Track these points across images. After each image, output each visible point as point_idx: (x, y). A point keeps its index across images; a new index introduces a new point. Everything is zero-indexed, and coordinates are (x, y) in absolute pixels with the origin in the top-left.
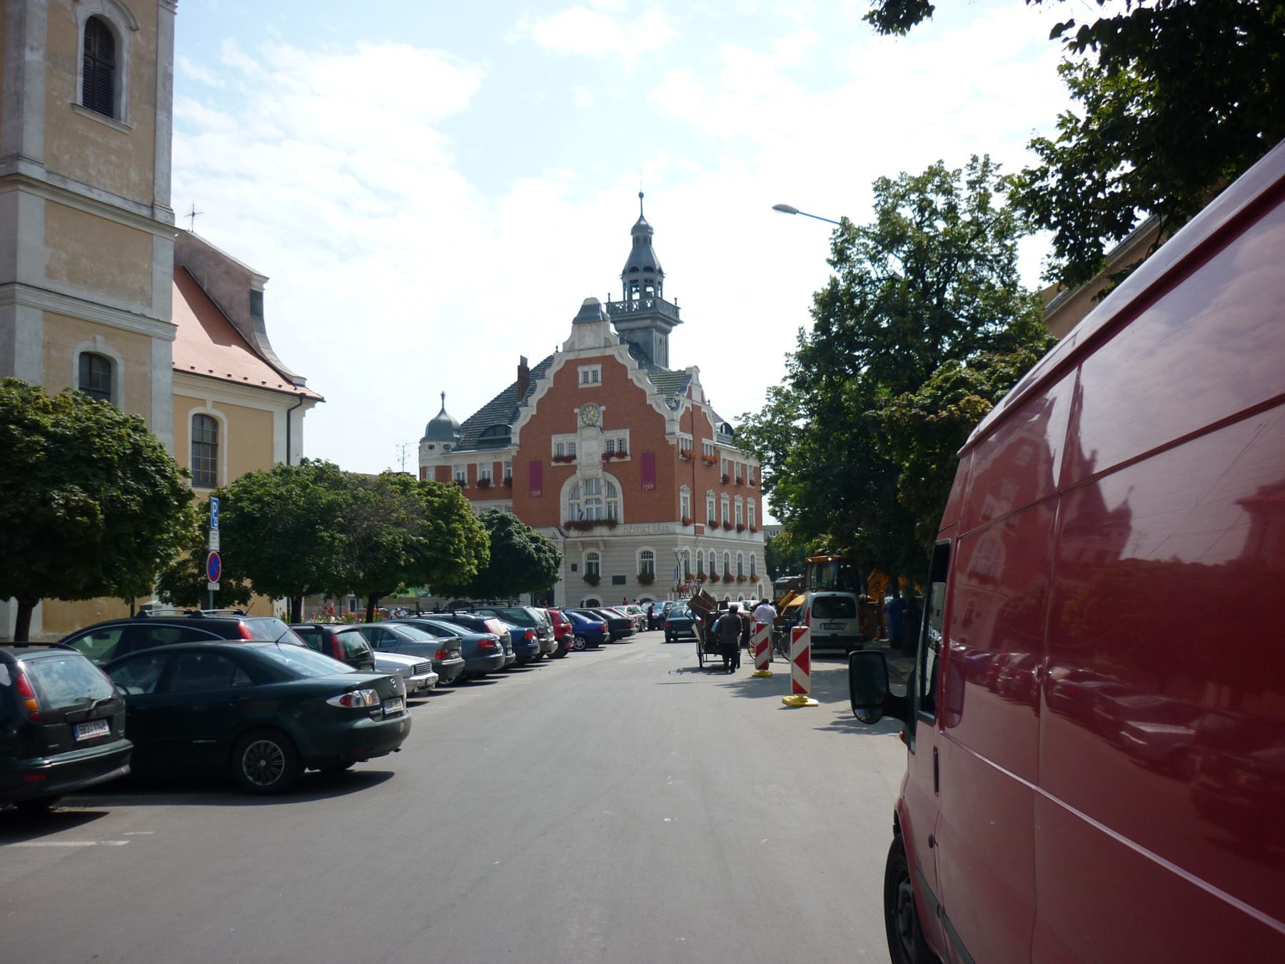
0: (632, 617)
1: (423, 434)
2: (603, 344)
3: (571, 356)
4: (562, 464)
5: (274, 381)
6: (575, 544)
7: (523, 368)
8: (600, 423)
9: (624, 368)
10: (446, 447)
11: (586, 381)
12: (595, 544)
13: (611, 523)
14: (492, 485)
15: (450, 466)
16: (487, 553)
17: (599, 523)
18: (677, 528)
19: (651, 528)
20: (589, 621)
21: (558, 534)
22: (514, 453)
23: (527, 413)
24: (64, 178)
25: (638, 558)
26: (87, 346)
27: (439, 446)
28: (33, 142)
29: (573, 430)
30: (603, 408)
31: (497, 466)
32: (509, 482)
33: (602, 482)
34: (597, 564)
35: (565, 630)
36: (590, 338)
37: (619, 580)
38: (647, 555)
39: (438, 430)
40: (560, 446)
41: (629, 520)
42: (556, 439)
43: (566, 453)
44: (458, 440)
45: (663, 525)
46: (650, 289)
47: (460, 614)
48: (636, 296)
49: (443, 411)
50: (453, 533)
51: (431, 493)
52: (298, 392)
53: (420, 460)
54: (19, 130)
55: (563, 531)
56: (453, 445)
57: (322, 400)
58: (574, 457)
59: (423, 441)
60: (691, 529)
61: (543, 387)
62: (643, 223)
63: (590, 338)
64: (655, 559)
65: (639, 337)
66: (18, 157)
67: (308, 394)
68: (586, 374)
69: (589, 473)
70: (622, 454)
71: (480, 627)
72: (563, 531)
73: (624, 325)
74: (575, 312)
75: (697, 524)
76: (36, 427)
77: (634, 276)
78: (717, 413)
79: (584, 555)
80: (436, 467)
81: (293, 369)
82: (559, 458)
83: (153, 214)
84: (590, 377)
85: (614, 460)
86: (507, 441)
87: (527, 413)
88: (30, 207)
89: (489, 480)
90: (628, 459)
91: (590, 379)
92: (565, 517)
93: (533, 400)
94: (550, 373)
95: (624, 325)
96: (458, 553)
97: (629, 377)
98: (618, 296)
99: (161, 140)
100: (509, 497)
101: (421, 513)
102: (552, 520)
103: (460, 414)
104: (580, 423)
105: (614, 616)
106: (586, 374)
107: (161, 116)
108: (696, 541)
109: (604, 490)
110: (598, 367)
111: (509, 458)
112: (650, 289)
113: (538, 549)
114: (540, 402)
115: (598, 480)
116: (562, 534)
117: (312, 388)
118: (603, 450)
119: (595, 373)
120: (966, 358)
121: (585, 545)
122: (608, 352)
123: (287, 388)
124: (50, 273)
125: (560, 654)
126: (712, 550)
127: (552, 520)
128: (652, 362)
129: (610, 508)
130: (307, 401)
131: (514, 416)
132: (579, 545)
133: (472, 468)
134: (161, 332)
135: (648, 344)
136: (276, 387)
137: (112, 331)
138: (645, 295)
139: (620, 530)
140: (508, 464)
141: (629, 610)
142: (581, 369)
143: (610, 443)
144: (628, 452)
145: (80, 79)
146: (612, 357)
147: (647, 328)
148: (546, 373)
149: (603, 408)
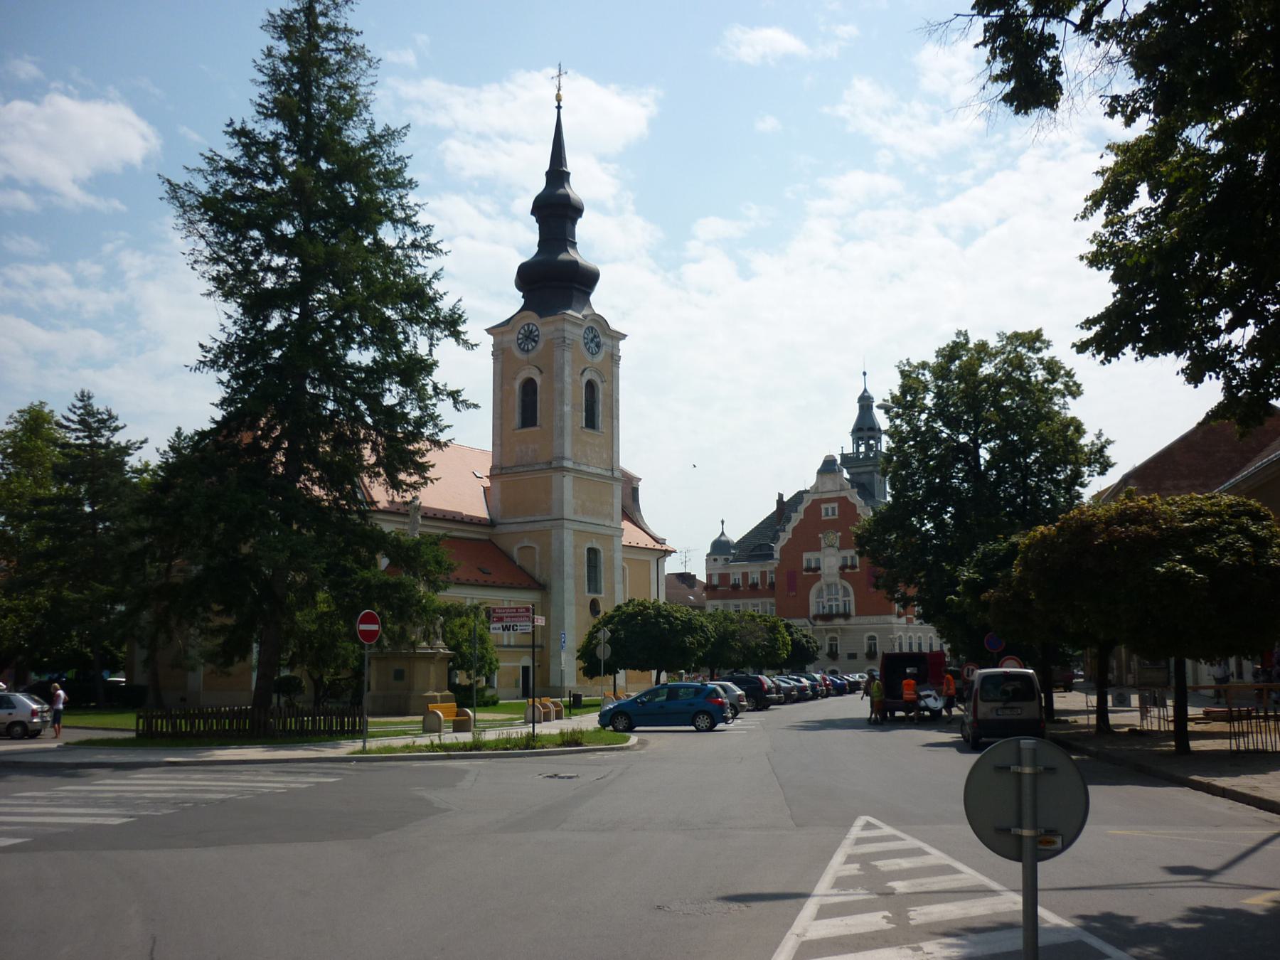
0: (861, 680)
1: (709, 551)
2: (838, 488)
3: (816, 497)
4: (810, 573)
5: (651, 544)
6: (821, 630)
7: (780, 501)
8: (837, 544)
9: (854, 506)
10: (726, 560)
11: (827, 514)
12: (835, 631)
13: (846, 616)
14: (760, 587)
15: (729, 574)
16: (790, 648)
17: (838, 615)
18: (894, 619)
19: (874, 619)
20: (839, 681)
21: (808, 624)
22: (776, 565)
23: (785, 537)
24: (579, 464)
25: (865, 640)
26: (589, 545)
27: (721, 559)
28: (568, 452)
29: (819, 549)
30: (840, 534)
31: (763, 574)
32: (772, 585)
33: (839, 587)
34: (837, 645)
35: (829, 685)
36: (830, 484)
37: (852, 656)
38: (872, 638)
39: (720, 547)
40: (809, 561)
41: (860, 613)
42: (806, 556)
43: (813, 565)
44: (734, 554)
45: (883, 618)
46: (872, 442)
47: (790, 676)
48: (862, 449)
49: (723, 534)
50: (776, 639)
51: (765, 620)
52: (664, 548)
53: (707, 568)
54: (562, 446)
55: (812, 620)
56: (731, 558)
57: (675, 552)
58: (819, 569)
59: (708, 555)
60: (903, 620)
61: (797, 518)
62: (866, 394)
63: (830, 484)
64: (877, 641)
65: (864, 479)
66: (563, 458)
67: (669, 549)
68: (827, 509)
69: (831, 580)
70: (853, 567)
71: (799, 681)
72: (812, 620)
73: (854, 470)
74: (819, 465)
75: (908, 616)
76: (676, 618)
77: (860, 434)
78: (822, 719)
79: (827, 638)
80: (719, 574)
81: (659, 534)
82: (808, 569)
83: (613, 474)
84: (830, 512)
85: (848, 571)
86: (771, 557)
87: (785, 537)
88: (568, 481)
89: (757, 584)
90: (858, 570)
91: (830, 513)
92: (813, 610)
93: (790, 527)
94: (801, 508)
95: (854, 470)
96: (779, 649)
97: (858, 512)
98: (849, 449)
99: (615, 436)
100: (772, 596)
101: (761, 629)
102: (805, 614)
103: (735, 535)
104: (823, 545)
105: (851, 680)
106: (827, 509)
107: (615, 421)
108: (907, 628)
109: (841, 592)
110: (836, 505)
111: (772, 568)
112: (872, 442)
113: (807, 642)
114: (795, 529)
115: (836, 585)
116: (811, 623)
117: (670, 545)
118: (839, 564)
119: (833, 509)
120: (1060, 529)
121: (827, 631)
122: (843, 494)
123: (658, 546)
124: (576, 512)
125: (826, 696)
126: (920, 634)
127: (805, 614)
128: (874, 497)
129: (845, 605)
130: (668, 553)
131: (775, 538)
132: (824, 631)
133: (745, 575)
134: (617, 533)
135: (872, 484)
136: (652, 547)
137: (599, 536)
138: (869, 447)
139: (853, 620)
140: (771, 572)
141: (860, 677)
142: (823, 506)
143: (845, 558)
144: (858, 565)
145: (584, 414)
146: (845, 498)
147: (871, 473)
148: (799, 508)
149: (840, 534)
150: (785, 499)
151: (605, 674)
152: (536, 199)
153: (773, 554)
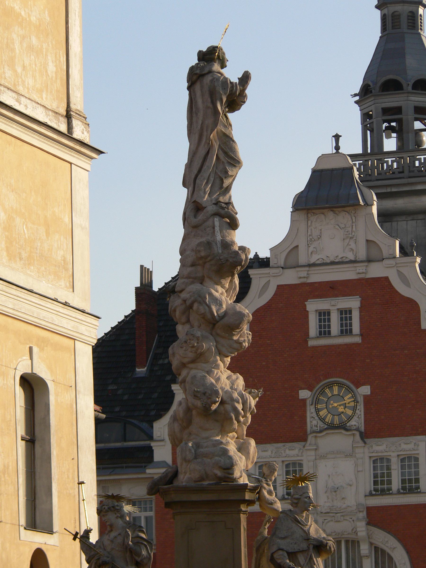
2: (362, 254)
30: (365, 390)
33: (364, 549)
91: (335, 328)
149: (365, 390)
150: (157, 286)
151: (151, 438)
152: (198, 54)
153: (150, 451)
